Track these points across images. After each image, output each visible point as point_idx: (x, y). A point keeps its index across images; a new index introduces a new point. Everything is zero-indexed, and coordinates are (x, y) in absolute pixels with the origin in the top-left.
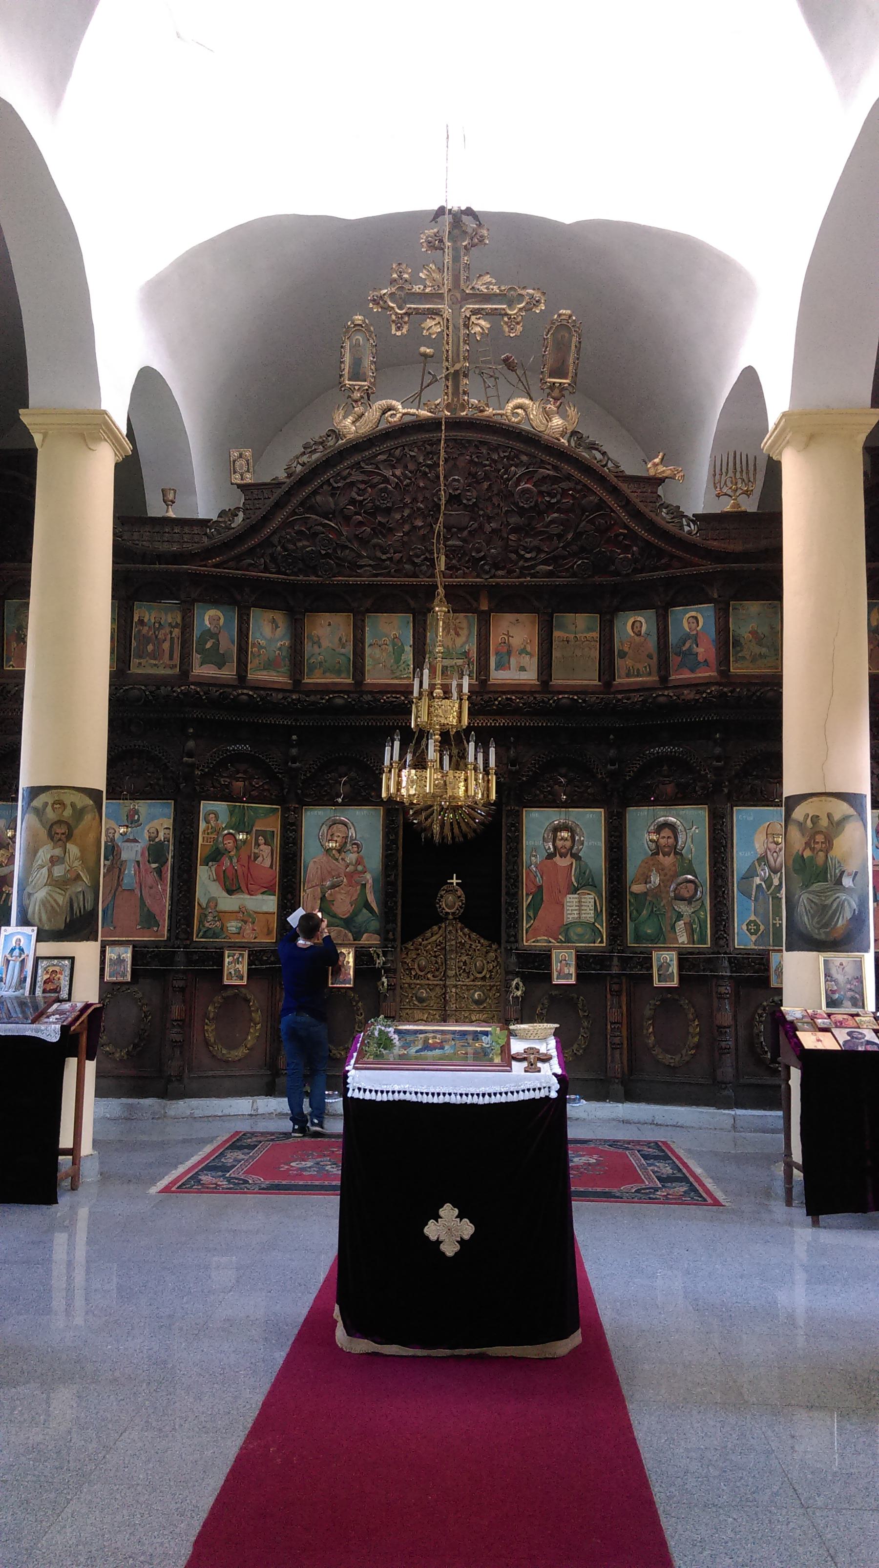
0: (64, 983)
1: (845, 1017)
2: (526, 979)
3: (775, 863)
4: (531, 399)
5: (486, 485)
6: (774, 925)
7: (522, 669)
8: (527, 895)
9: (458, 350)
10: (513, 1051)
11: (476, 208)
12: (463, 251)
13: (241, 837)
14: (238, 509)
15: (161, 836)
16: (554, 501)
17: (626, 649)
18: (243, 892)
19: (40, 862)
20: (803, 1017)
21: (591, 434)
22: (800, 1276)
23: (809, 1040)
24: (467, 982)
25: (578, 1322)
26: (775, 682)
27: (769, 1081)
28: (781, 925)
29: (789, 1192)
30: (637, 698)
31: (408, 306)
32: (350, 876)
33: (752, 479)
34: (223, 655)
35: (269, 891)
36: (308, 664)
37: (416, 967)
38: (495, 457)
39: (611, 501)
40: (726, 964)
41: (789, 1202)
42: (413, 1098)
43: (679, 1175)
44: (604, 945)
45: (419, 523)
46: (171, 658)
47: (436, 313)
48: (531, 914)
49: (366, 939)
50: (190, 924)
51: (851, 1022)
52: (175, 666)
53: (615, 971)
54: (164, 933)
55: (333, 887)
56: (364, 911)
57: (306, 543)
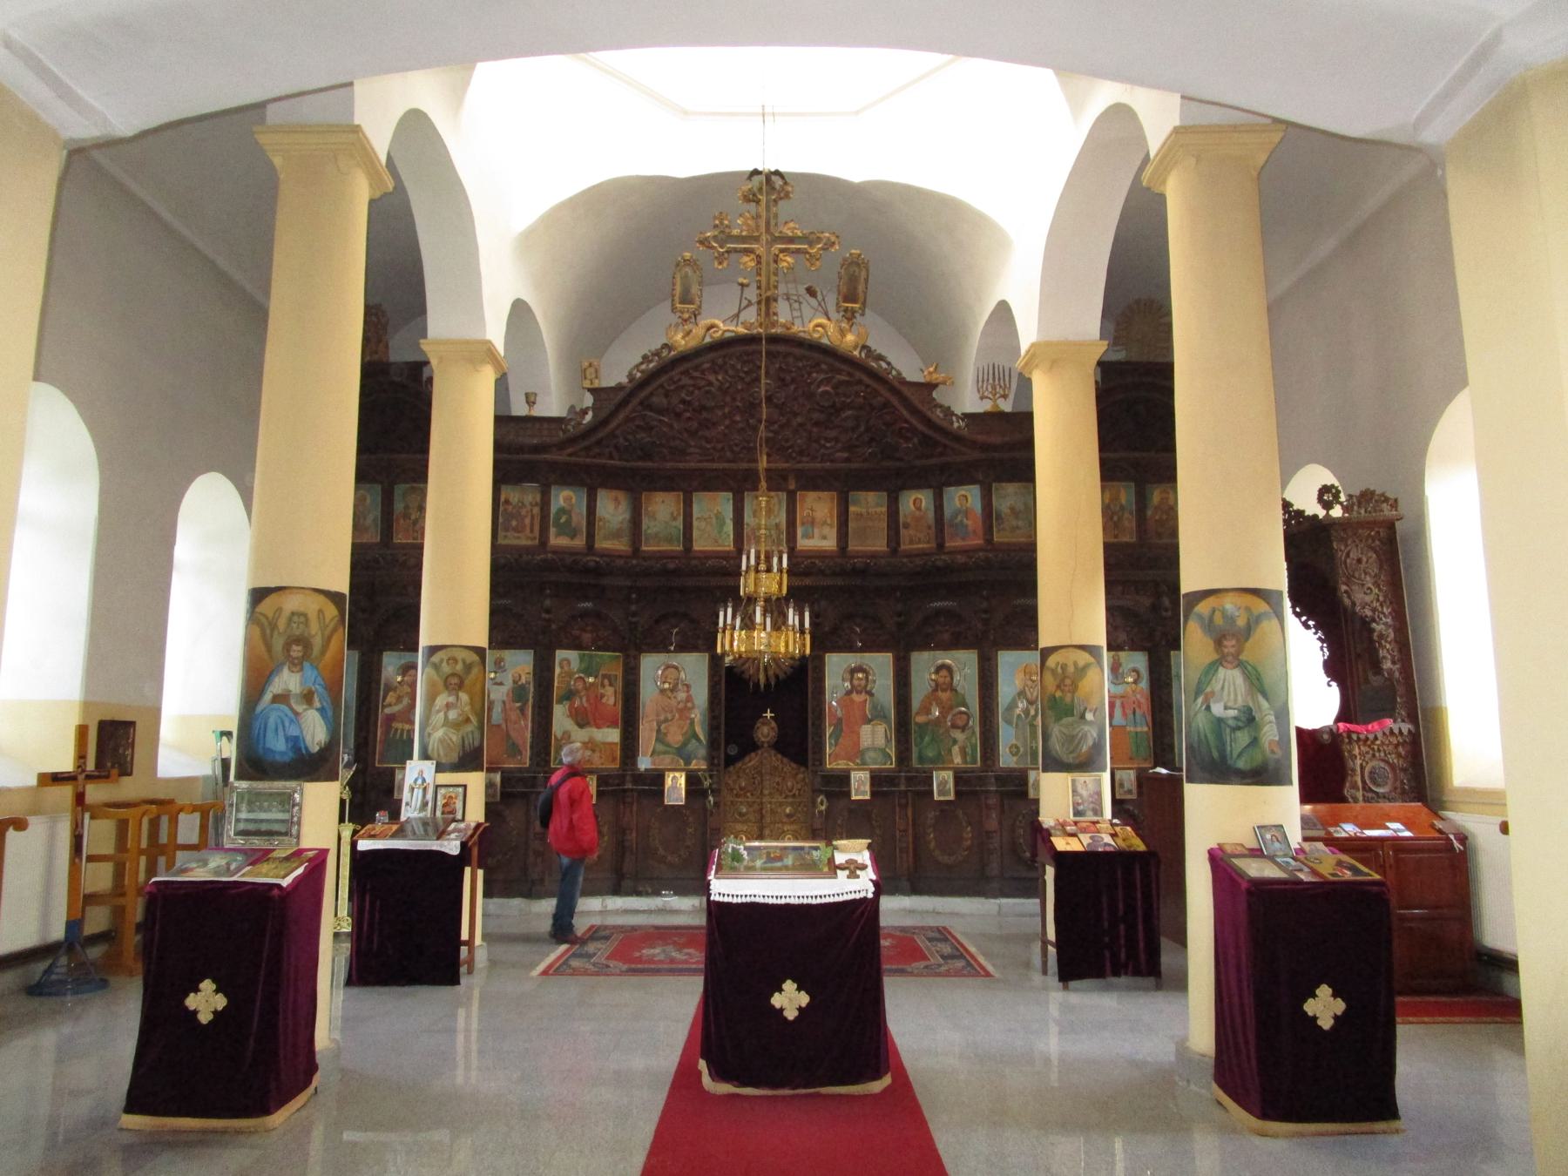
0: (459, 805)
1: (1088, 824)
2: (829, 796)
3: (1032, 694)
4: (829, 319)
5: (792, 387)
6: (1032, 747)
7: (824, 538)
8: (830, 725)
9: (769, 280)
10: (837, 862)
11: (782, 169)
12: (772, 203)
13: (591, 680)
14: (588, 408)
15: (523, 680)
16: (849, 401)
17: (909, 520)
18: (591, 726)
19: (437, 708)
20: (1056, 825)
21: (878, 347)
22: (1054, 1029)
23: (1061, 844)
24: (781, 799)
25: (889, 1067)
26: (1031, 548)
27: (1032, 874)
28: (1037, 747)
29: (1045, 963)
30: (918, 561)
31: (728, 246)
32: (681, 711)
33: (1008, 386)
34: (574, 529)
35: (613, 724)
36: (645, 535)
37: (737, 787)
38: (800, 364)
39: (895, 401)
40: (993, 780)
41: (1045, 972)
42: (761, 900)
43: (958, 953)
44: (893, 766)
45: (738, 418)
46: (532, 531)
47: (751, 251)
48: (833, 742)
49: (693, 766)
50: (549, 754)
51: (1092, 828)
52: (535, 538)
53: (903, 788)
54: (526, 760)
55: (666, 720)
56: (694, 741)
57: (644, 435)
